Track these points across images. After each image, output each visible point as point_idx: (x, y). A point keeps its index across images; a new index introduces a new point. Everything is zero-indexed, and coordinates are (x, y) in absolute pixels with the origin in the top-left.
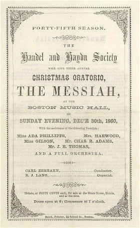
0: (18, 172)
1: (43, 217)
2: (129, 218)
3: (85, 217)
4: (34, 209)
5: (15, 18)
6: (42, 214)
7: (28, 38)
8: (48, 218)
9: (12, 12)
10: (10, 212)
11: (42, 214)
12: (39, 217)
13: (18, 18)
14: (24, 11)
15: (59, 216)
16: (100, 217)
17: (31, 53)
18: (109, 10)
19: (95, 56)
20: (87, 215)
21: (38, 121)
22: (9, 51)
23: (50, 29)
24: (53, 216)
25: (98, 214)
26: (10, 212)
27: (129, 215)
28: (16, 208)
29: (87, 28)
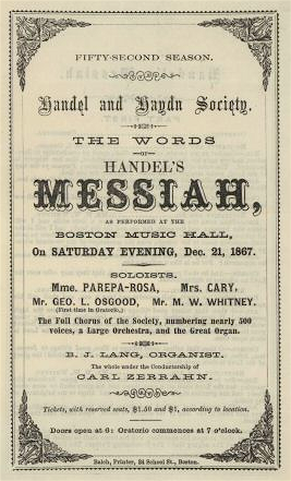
0: (28, 368)
1: (89, 462)
2: (15, 16)
3: (181, 462)
4: (68, 444)
5: (33, 33)
6: (86, 457)
7: (52, 66)
8: (101, 465)
9: (269, 458)
10: (273, 28)
11: (86, 457)
12: (81, 463)
13: (257, 447)
14: (243, 460)
15: (124, 459)
16: (212, 463)
17: (57, 96)
18: (231, 17)
19: (200, 103)
20: (184, 459)
21: (106, 252)
22: (14, 107)
23: (102, 58)
24: (111, 460)
25: (208, 456)
26: (273, 28)
27: (15, 21)
28: (33, 445)
29: (181, 57)
